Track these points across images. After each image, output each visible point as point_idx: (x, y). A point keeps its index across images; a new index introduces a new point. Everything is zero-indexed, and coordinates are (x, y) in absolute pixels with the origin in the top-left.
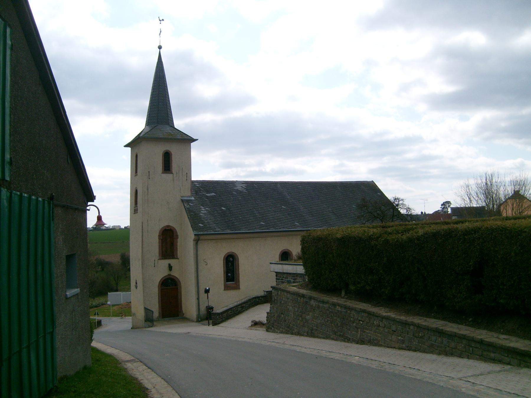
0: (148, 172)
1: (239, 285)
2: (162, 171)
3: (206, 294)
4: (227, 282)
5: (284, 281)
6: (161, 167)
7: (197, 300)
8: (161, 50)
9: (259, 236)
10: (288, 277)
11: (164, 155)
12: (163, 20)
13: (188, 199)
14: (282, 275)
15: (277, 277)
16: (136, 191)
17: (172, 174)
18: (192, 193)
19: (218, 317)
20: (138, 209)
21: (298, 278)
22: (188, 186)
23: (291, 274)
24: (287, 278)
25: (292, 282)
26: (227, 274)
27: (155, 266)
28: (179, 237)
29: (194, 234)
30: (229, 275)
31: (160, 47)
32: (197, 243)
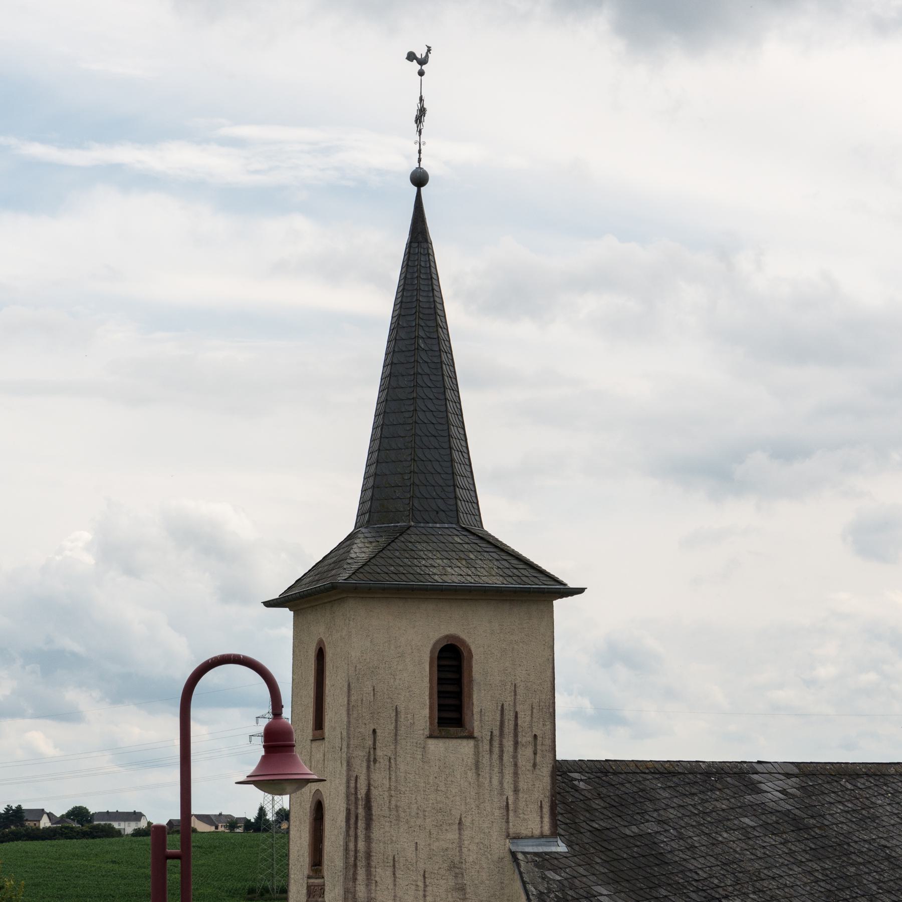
0: (371, 732)
6: (426, 712)
8: (422, 189)
11: (439, 658)
12: (411, 57)
13: (540, 849)
17: (471, 743)
18: (554, 824)
31: (419, 179)
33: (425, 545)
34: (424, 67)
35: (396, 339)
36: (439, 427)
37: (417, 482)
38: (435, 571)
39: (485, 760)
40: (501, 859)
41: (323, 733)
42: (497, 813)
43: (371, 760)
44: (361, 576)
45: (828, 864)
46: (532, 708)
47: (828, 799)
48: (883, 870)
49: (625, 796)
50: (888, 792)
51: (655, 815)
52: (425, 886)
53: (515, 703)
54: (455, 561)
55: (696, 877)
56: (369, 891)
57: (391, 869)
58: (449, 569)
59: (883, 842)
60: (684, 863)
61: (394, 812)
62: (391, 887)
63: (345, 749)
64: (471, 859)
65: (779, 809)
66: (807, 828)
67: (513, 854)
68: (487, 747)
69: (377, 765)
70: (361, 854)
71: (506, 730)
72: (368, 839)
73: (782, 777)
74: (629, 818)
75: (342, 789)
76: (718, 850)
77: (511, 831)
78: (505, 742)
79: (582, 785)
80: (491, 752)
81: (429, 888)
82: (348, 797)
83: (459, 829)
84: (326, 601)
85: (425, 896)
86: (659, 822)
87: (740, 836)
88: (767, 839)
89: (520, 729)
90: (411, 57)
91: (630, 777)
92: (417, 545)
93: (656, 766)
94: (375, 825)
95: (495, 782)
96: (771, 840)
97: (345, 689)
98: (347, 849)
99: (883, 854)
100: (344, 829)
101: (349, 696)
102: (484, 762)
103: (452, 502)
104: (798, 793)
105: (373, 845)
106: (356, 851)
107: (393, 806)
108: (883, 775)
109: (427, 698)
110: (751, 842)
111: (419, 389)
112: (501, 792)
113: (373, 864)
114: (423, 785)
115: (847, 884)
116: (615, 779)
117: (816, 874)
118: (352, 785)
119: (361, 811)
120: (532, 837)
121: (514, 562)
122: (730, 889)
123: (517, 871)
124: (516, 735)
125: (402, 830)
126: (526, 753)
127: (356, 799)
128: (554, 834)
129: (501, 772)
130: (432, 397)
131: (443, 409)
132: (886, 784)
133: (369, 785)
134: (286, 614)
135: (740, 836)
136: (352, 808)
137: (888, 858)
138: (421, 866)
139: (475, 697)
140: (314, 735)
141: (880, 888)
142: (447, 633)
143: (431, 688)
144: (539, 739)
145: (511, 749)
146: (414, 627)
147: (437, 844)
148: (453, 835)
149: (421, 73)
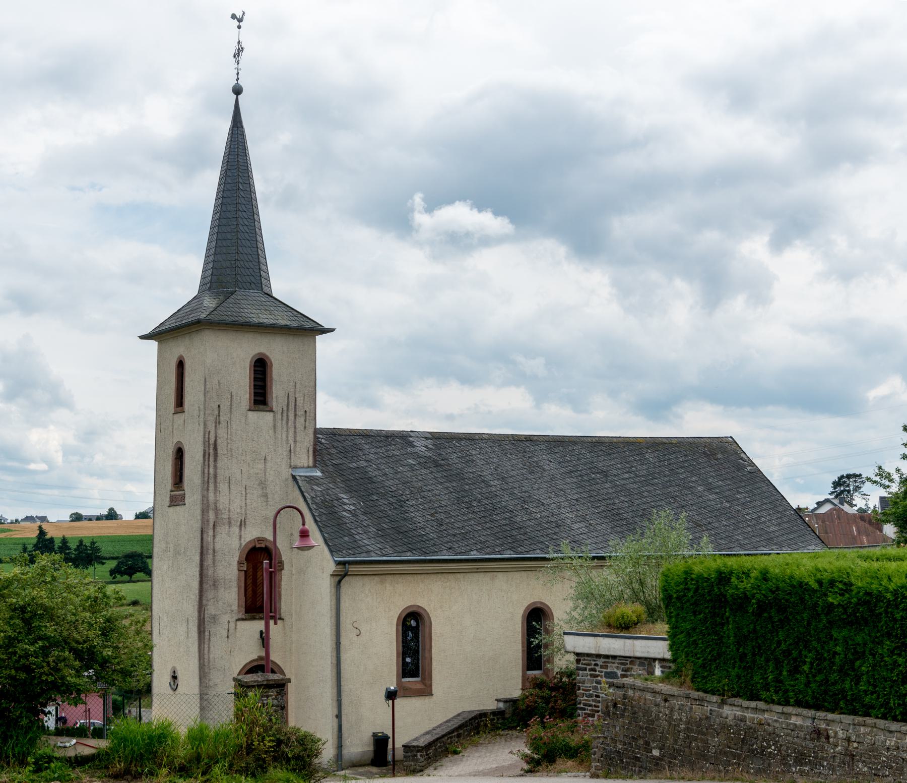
1: (431, 686)
2: (250, 406)
3: (391, 702)
4: (403, 677)
5: (597, 673)
6: (248, 396)
7: (336, 720)
9: (478, 569)
10: (609, 665)
11: (255, 366)
12: (234, 16)
13: (308, 474)
14: (594, 661)
15: (580, 665)
16: (179, 454)
17: (272, 414)
18: (315, 461)
19: (419, 756)
20: (187, 496)
21: (635, 667)
22: (306, 441)
23: (618, 658)
24: (606, 667)
25: (619, 675)
26: (404, 659)
27: (228, 637)
28: (286, 567)
29: (335, 561)
30: (408, 660)
31: (237, 91)
32: (339, 582)
33: (246, 301)
34: (241, 24)
35: (225, 183)
36: (251, 235)
37: (239, 265)
38: (253, 316)
39: (279, 424)
40: (287, 479)
41: (183, 409)
42: (285, 453)
43: (217, 422)
44: (212, 316)
45: (455, 484)
46: (304, 396)
47: (448, 451)
48: (482, 487)
49: (347, 447)
50: (477, 448)
51: (364, 457)
52: (246, 494)
53: (295, 393)
54: (263, 311)
55: (391, 490)
56: (216, 496)
57: (227, 484)
58: (261, 315)
59: (479, 473)
60: (383, 482)
61: (229, 452)
62: (228, 494)
63: (202, 416)
64: (270, 479)
65: (425, 455)
66: (441, 466)
67: (294, 477)
68: (280, 417)
69: (221, 425)
70: (211, 476)
71: (290, 408)
72: (215, 467)
73: (424, 439)
74: (351, 459)
75: (201, 439)
76: (398, 476)
77: (292, 464)
78: (289, 414)
79: (323, 441)
80: (282, 419)
81: (248, 495)
82: (204, 443)
83: (265, 462)
84: (194, 330)
85: (246, 499)
86: (367, 461)
87: (409, 469)
88: (422, 471)
89: (297, 407)
90: (234, 16)
91: (347, 437)
92: (241, 301)
93: (360, 432)
94: (219, 459)
95: (284, 436)
96: (424, 471)
97: (203, 382)
98: (203, 473)
99: (480, 479)
100: (202, 462)
101: (205, 386)
102: (278, 425)
103: (259, 278)
104: (434, 448)
105: (218, 470)
106: (209, 474)
107: (229, 449)
108: (473, 440)
109: (248, 388)
110: (415, 472)
111: (240, 213)
112: (287, 443)
113: (218, 481)
114: (245, 437)
115: (466, 494)
116: (340, 438)
117: (450, 489)
118: (207, 436)
119: (212, 451)
120: (303, 467)
121: (295, 313)
122: (409, 496)
123: (296, 486)
124: (295, 411)
125: (233, 463)
126: (301, 420)
127: (209, 444)
128: (315, 466)
129: (287, 431)
130: (247, 217)
131: (253, 225)
132: (475, 444)
133: (216, 437)
134: (153, 345)
135: (409, 469)
136: (207, 449)
137: (483, 481)
138: (244, 483)
139: (274, 388)
140: (175, 411)
141: (482, 496)
142: (259, 352)
143: (250, 382)
144: (308, 413)
145: (293, 418)
146: (241, 347)
147: (252, 470)
148: (261, 466)
149: (239, 27)
